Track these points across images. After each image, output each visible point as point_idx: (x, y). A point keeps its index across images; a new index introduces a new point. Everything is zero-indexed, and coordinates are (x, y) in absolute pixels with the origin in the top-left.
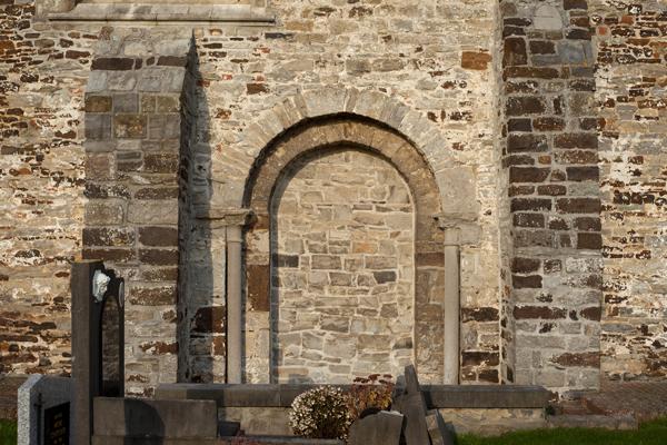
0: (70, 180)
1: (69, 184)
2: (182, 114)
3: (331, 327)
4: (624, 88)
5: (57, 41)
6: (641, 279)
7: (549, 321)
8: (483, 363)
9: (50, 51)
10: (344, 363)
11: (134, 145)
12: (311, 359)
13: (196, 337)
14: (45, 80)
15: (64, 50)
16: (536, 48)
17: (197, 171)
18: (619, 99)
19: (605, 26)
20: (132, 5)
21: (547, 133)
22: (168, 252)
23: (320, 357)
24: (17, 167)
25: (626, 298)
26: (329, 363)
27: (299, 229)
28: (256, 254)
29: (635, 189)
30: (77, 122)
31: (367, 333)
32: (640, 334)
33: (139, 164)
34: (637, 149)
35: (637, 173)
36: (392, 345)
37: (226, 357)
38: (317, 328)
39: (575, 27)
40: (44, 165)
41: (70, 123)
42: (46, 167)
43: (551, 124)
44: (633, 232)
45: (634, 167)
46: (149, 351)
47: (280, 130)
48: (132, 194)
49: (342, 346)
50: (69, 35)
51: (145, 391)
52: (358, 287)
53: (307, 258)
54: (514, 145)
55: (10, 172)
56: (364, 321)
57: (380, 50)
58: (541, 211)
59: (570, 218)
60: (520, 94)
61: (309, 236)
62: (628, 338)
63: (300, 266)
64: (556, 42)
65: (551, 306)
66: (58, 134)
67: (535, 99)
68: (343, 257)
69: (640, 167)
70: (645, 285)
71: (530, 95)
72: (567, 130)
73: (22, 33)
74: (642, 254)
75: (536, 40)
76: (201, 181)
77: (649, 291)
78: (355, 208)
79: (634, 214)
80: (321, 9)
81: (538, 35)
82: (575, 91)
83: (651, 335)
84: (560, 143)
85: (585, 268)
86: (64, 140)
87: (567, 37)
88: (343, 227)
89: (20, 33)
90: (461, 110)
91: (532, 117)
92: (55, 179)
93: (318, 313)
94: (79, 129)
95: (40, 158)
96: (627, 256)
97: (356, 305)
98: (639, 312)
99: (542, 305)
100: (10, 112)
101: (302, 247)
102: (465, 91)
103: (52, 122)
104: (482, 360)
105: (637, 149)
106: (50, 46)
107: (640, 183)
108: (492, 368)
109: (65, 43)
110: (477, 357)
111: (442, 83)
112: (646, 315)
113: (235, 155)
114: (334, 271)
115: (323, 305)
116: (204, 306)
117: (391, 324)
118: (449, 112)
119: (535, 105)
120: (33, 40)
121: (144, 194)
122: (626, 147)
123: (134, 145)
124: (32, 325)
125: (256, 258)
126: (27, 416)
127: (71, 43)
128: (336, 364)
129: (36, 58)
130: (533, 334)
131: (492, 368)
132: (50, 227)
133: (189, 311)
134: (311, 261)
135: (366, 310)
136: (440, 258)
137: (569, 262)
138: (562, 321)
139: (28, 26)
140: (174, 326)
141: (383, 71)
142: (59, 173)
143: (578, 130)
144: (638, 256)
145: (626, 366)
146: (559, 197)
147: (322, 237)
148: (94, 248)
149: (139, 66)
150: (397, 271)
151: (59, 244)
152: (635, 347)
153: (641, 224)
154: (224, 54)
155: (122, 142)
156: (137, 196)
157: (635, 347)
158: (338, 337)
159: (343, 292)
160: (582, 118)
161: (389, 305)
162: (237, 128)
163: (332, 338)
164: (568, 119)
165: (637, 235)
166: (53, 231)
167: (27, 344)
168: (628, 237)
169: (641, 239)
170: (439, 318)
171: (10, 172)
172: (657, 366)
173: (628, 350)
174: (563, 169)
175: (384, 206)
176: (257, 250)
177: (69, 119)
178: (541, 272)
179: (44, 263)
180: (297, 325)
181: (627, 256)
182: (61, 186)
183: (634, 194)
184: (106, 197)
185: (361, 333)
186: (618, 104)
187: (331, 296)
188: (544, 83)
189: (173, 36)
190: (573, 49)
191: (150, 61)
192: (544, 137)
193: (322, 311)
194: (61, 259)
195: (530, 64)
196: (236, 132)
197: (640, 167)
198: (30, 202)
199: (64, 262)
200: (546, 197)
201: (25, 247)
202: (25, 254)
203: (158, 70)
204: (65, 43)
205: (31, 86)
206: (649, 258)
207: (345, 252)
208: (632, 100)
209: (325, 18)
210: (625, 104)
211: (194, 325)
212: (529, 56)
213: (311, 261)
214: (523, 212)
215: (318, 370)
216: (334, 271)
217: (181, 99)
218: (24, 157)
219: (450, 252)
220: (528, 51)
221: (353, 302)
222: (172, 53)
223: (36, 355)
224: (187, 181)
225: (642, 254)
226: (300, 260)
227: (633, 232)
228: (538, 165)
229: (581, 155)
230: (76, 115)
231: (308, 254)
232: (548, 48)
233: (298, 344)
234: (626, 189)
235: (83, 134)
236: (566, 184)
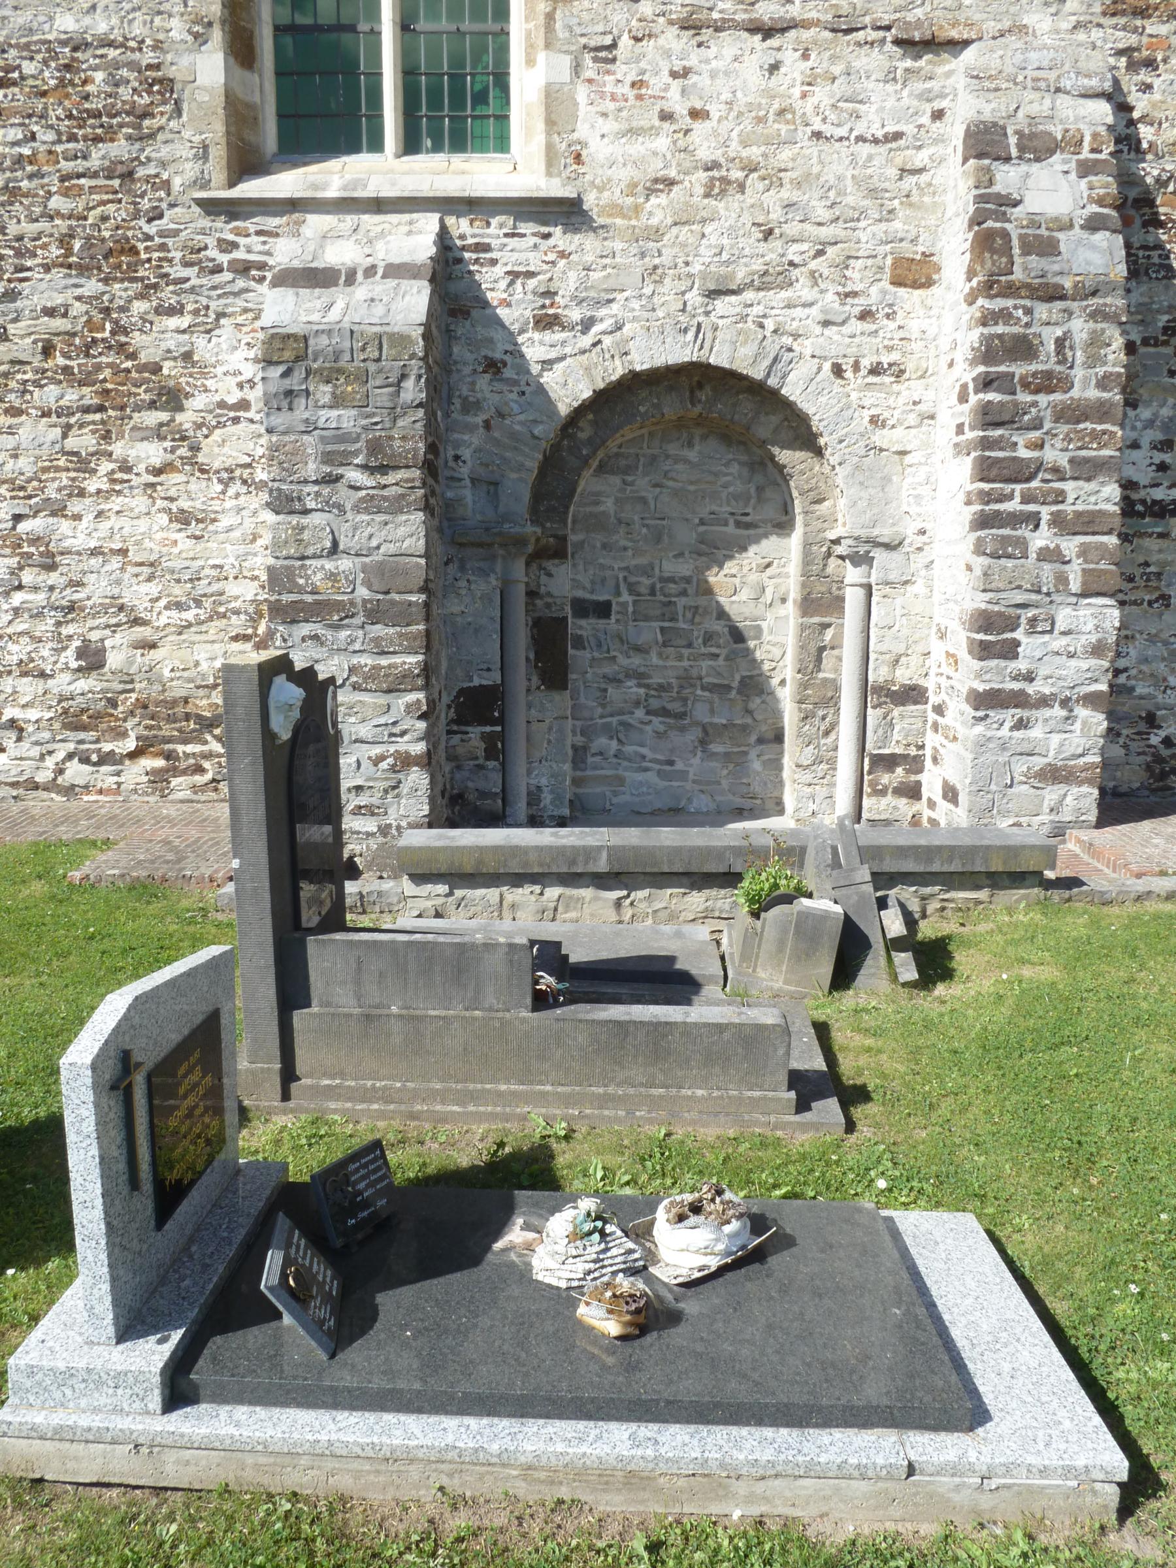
0: (245, 482)
1: (244, 489)
2: (427, 363)
3: (664, 712)
4: (1155, 321)
5: (211, 241)
6: (1152, 639)
7: (1026, 714)
8: (899, 770)
9: (201, 261)
10: (679, 766)
11: (346, 419)
12: (630, 761)
13: (455, 733)
14: (196, 312)
15: (224, 259)
16: (1028, 248)
17: (451, 463)
18: (1145, 342)
19: (1132, 212)
20: (336, 177)
21: (1043, 399)
22: (410, 604)
23: (644, 757)
24: (157, 462)
25: (1126, 670)
26: (658, 767)
27: (614, 558)
28: (549, 600)
29: (1159, 494)
30: (251, 383)
31: (716, 720)
32: (1142, 726)
33: (356, 453)
34: (1166, 427)
35: (1162, 467)
36: (753, 738)
37: (503, 764)
38: (640, 713)
39: (1095, 208)
40: (201, 459)
41: (240, 386)
42: (205, 461)
43: (1047, 383)
44: (1147, 564)
45: (1159, 457)
46: (384, 765)
47: (587, 394)
48: (348, 507)
49: (676, 738)
50: (231, 231)
51: (379, 827)
52: (703, 650)
53: (624, 605)
54: (988, 417)
55: (148, 471)
56: (711, 703)
57: (761, 256)
58: (1024, 532)
59: (1070, 546)
60: (1000, 329)
61: (627, 568)
62: (1125, 732)
63: (613, 617)
64: (1061, 236)
65: (1031, 689)
66: (222, 405)
67: (1025, 336)
68: (681, 602)
69: (1167, 457)
70: (1159, 650)
71: (1016, 330)
72: (1075, 393)
73: (151, 229)
74: (1157, 600)
75: (1029, 231)
76: (460, 480)
77: (1164, 659)
78: (702, 522)
79: (1151, 535)
80: (656, 181)
81: (1034, 223)
82: (1091, 324)
83: (1160, 727)
84: (1065, 414)
85: (1090, 626)
86: (232, 414)
87: (1082, 227)
88: (681, 555)
89: (147, 228)
90: (885, 360)
91: (1019, 369)
92: (220, 481)
93: (642, 691)
94: (255, 395)
95: (196, 449)
96: (1135, 603)
97: (701, 679)
98: (1146, 691)
99: (1016, 686)
100: (141, 369)
101: (617, 586)
102: (892, 325)
103: (210, 383)
104: (898, 765)
105: (1166, 427)
106: (199, 250)
107: (1166, 484)
108: (913, 778)
109: (227, 246)
110: (889, 762)
111: (857, 310)
112: (1155, 697)
113: (514, 436)
114: (666, 624)
115: (649, 677)
116: (466, 685)
117: (752, 706)
118: (866, 363)
119: (1023, 348)
120: (170, 242)
121: (369, 505)
122: (1150, 424)
123: (346, 419)
124: (199, 718)
125: (548, 606)
126: (90, 1126)
127: (235, 245)
128: (668, 768)
129: (177, 272)
130: (999, 734)
131: (913, 778)
132: (217, 562)
133: (444, 694)
134: (631, 609)
135: (715, 685)
136: (837, 604)
137: (1064, 617)
138: (1046, 713)
139: (161, 216)
140: (422, 725)
141: (759, 289)
142: (226, 470)
143: (1093, 393)
144: (1150, 603)
145: (1119, 774)
146: (1054, 508)
147: (647, 570)
148: (286, 598)
149: (351, 279)
150: (764, 625)
151: (232, 588)
152: (1134, 746)
153: (1160, 551)
154: (494, 262)
155: (324, 414)
156: (357, 509)
157: (1134, 746)
158: (671, 727)
159: (680, 658)
160: (1101, 371)
161: (751, 677)
162: (516, 389)
163: (662, 728)
164: (1078, 373)
165: (1152, 569)
166: (221, 567)
167: (190, 748)
168: (1138, 572)
169: (1159, 575)
170: (832, 701)
171: (148, 471)
172: (1163, 776)
173: (1123, 751)
174: (1063, 461)
175: (747, 519)
176: (549, 594)
177: (240, 379)
178: (1018, 635)
179: (211, 619)
180: (609, 709)
181: (1135, 603)
182: (231, 491)
183: (1154, 502)
184: (306, 512)
185: (706, 720)
186: (1143, 350)
187: (661, 663)
188: (1042, 311)
189: (407, 228)
190: (1094, 248)
191: (370, 271)
192: (1035, 404)
193: (647, 686)
194: (237, 612)
195: (1018, 275)
196: (514, 396)
197: (1167, 457)
198: (183, 518)
199: (243, 617)
200: (1032, 508)
201: (178, 591)
202: (179, 606)
203: (380, 287)
204: (227, 246)
205: (173, 322)
206: (1168, 606)
207: (684, 593)
208: (1166, 343)
209: (663, 196)
210: (1152, 350)
211: (452, 714)
212: (1018, 260)
213: (631, 609)
214: (994, 531)
215: (640, 777)
216: (666, 624)
217: (424, 336)
218: (168, 444)
219: (853, 598)
220: (1016, 251)
221: (694, 673)
222: (406, 259)
223: (206, 765)
224: (437, 481)
225: (1157, 600)
226: (614, 607)
227: (1147, 564)
228: (1023, 453)
229: (1094, 435)
230: (250, 371)
231: (626, 597)
232: (1049, 248)
233: (611, 738)
234: (1142, 494)
235: (261, 404)
236: (1069, 486)
